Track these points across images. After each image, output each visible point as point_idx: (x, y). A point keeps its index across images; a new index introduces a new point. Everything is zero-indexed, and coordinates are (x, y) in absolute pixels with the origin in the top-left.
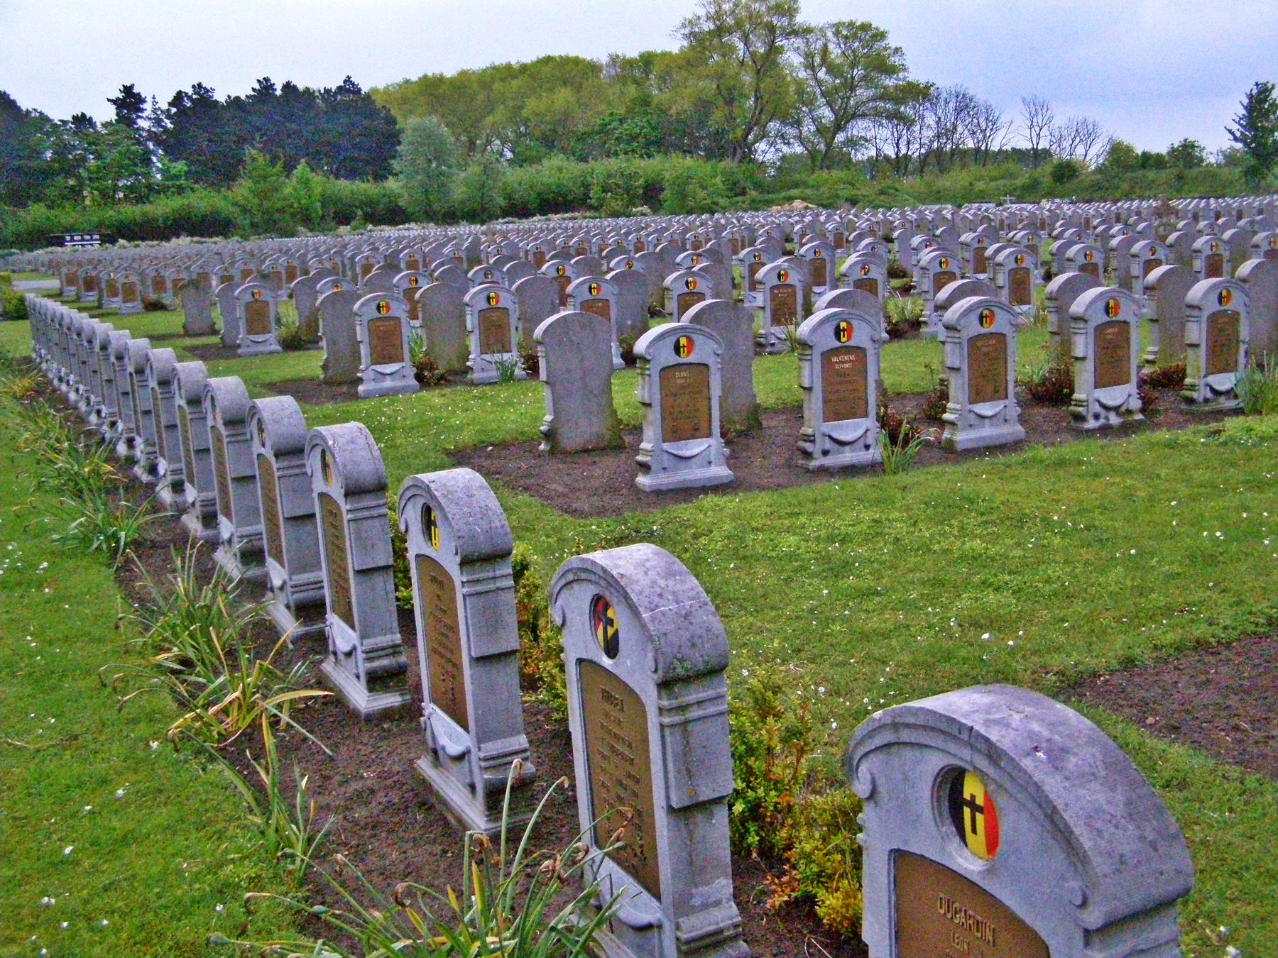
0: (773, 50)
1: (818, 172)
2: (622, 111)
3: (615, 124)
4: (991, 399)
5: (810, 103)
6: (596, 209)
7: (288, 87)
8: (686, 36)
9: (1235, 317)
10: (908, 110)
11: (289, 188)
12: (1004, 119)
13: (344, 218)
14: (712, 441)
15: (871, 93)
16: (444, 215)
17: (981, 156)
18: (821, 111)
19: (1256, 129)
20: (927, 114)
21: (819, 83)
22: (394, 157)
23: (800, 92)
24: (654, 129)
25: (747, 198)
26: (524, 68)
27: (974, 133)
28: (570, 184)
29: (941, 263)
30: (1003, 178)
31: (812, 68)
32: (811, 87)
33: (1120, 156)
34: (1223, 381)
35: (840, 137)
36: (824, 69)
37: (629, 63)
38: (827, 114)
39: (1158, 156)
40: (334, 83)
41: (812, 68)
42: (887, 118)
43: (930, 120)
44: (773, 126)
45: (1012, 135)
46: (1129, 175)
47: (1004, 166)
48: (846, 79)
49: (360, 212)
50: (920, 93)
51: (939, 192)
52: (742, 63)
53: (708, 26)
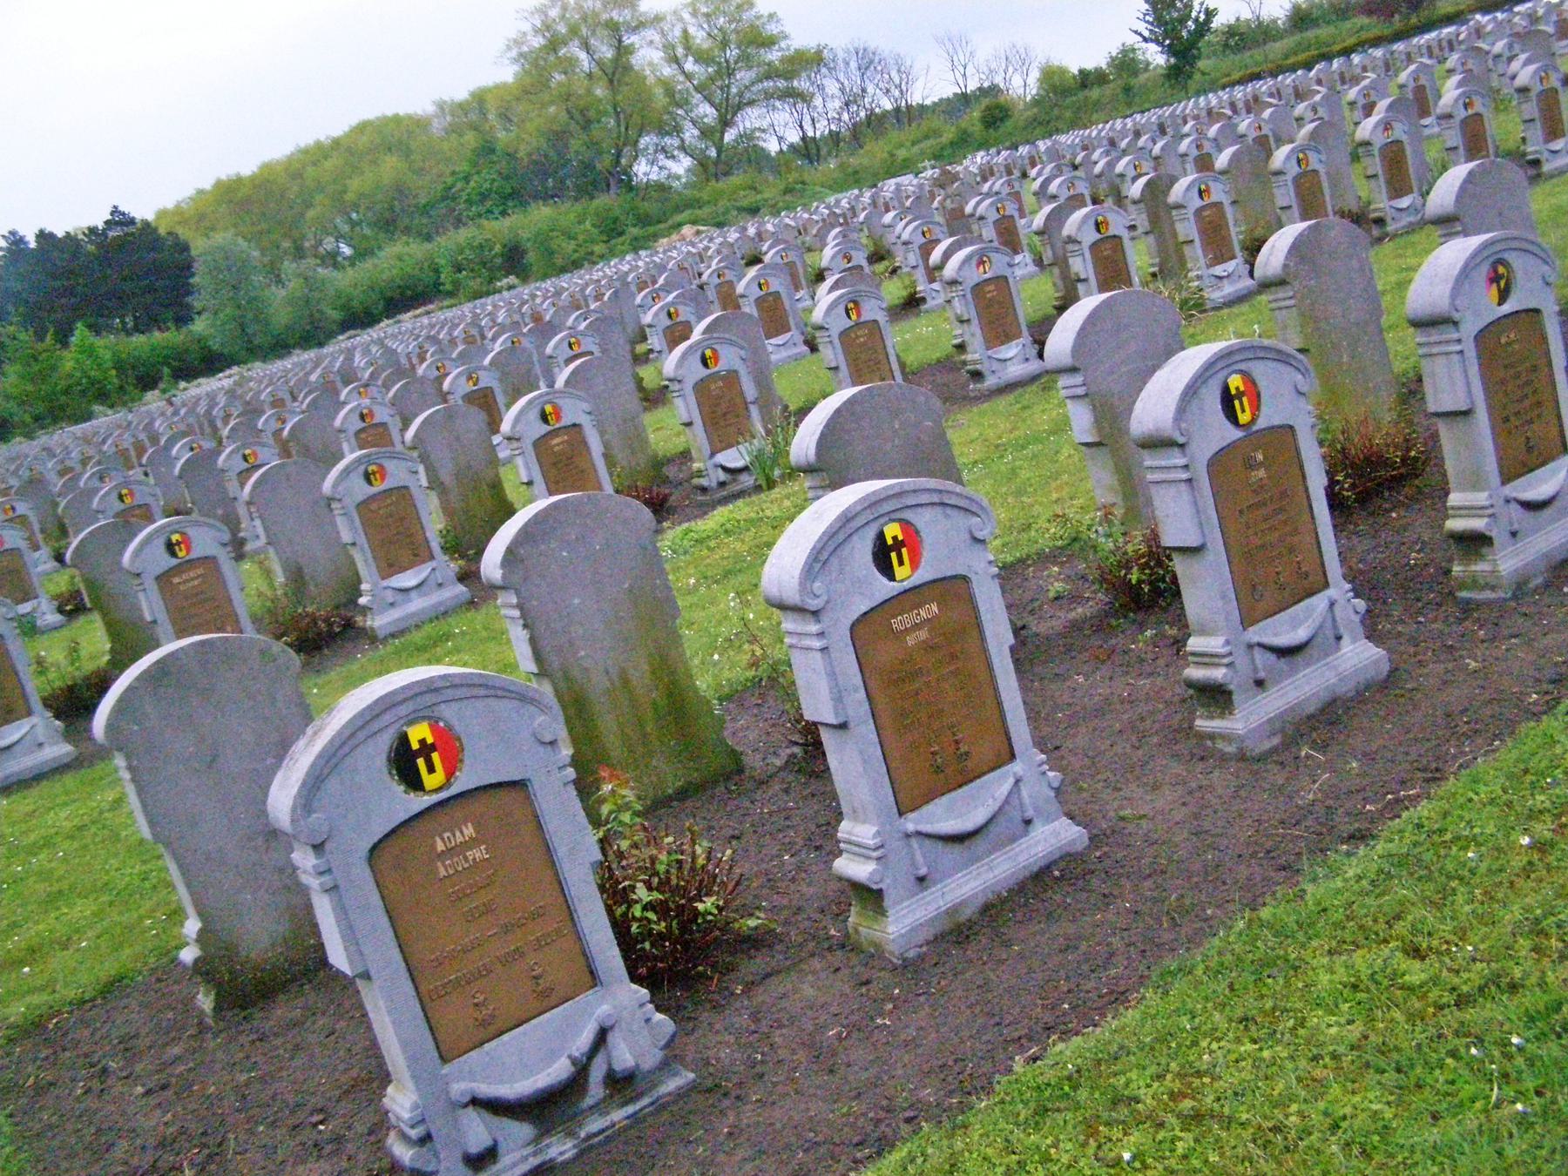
0: (623, 51)
3: (459, 185)
5: (684, 103)
6: (450, 294)
7: (43, 236)
8: (516, 60)
9: (732, 378)
10: (801, 84)
11: (68, 362)
13: (148, 382)
14: (34, 720)
17: (906, 115)
20: (826, 82)
22: (189, 293)
23: (670, 92)
24: (507, 178)
26: (336, 143)
28: (417, 272)
29: (570, 345)
30: (927, 137)
32: (681, 85)
34: (733, 457)
35: (730, 136)
37: (462, 107)
38: (707, 112)
40: (99, 219)
43: (832, 87)
45: (933, 85)
46: (1068, 101)
47: (925, 125)
50: (812, 61)
52: (590, 76)
53: (537, 42)
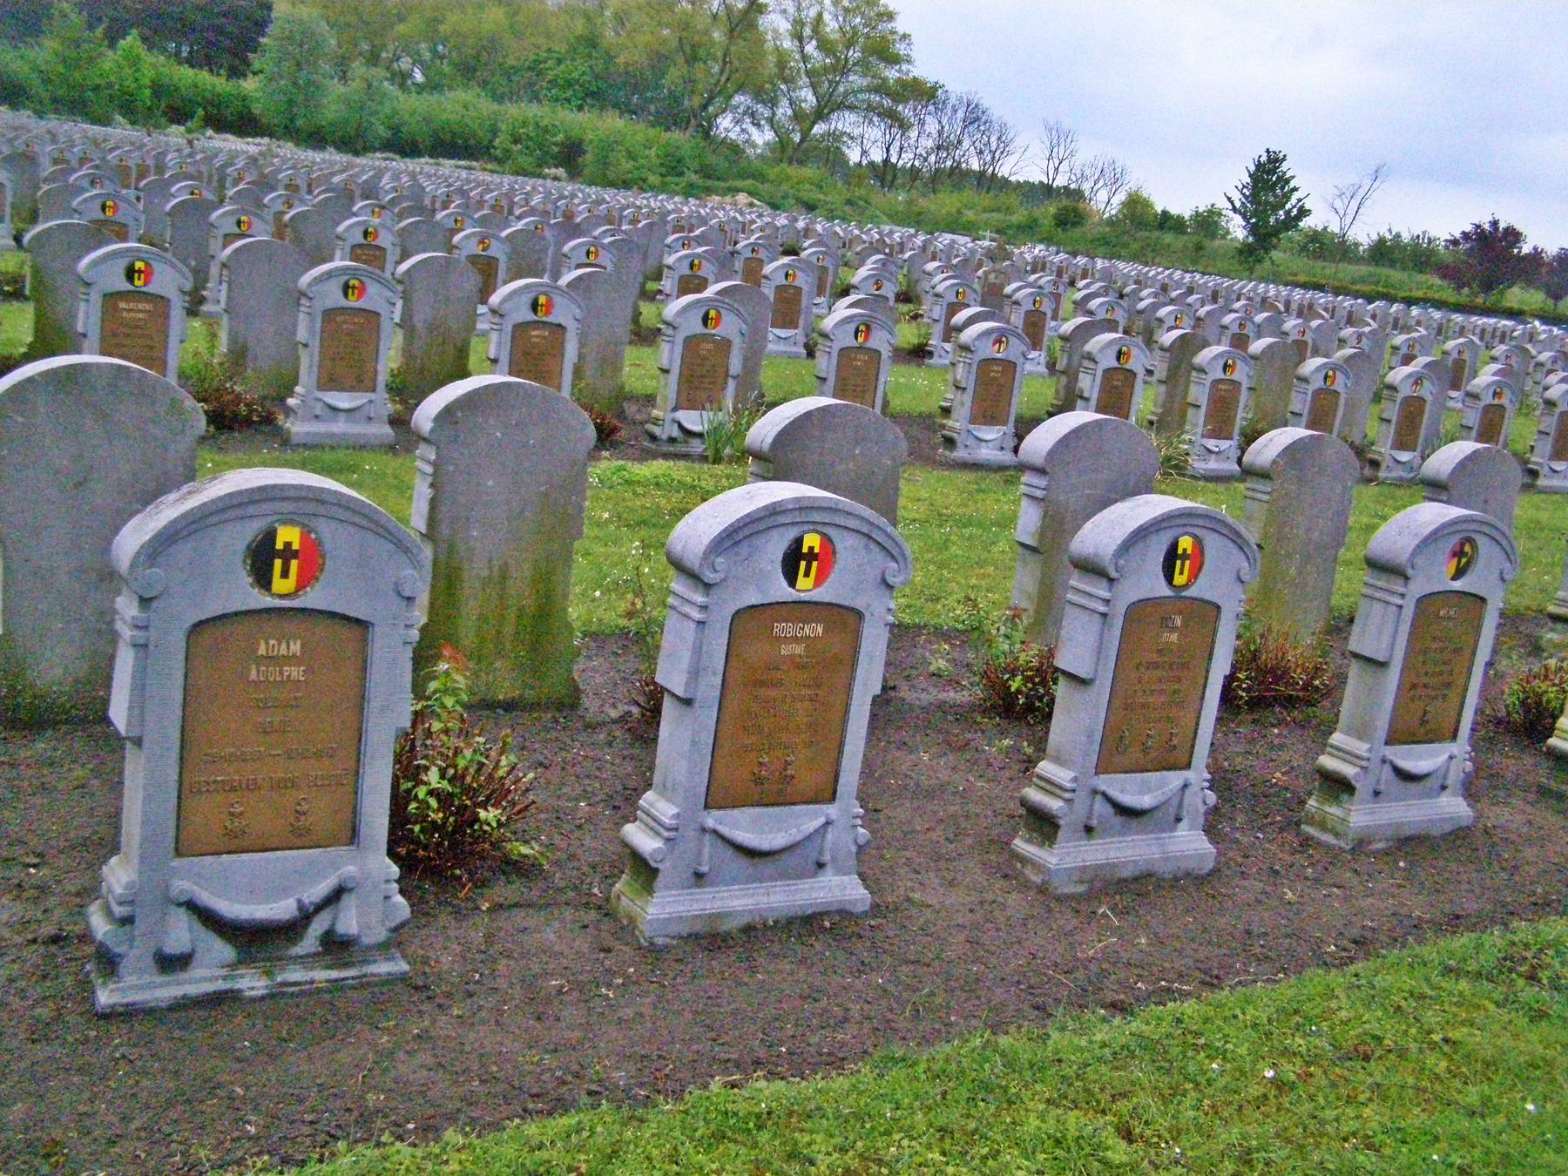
1: (784, 165)
2: (562, 48)
3: (550, 63)
4: (352, 389)
9: (725, 344)
10: (906, 111)
11: (109, 61)
12: (1019, 142)
13: (178, 115)
15: (865, 82)
16: (310, 135)
17: (987, 182)
18: (803, 94)
19: (1259, 204)
20: (929, 119)
21: (805, 58)
23: (782, 65)
24: (597, 77)
25: (683, 181)
27: (981, 152)
31: (800, 38)
33: (1137, 210)
34: (692, 420)
35: (819, 129)
36: (814, 42)
38: (808, 98)
39: (1180, 219)
41: (800, 38)
42: (879, 115)
43: (932, 126)
44: (740, 99)
47: (1003, 198)
48: (838, 59)
49: (200, 112)
50: (925, 93)
51: (920, 214)
52: (715, 16)
